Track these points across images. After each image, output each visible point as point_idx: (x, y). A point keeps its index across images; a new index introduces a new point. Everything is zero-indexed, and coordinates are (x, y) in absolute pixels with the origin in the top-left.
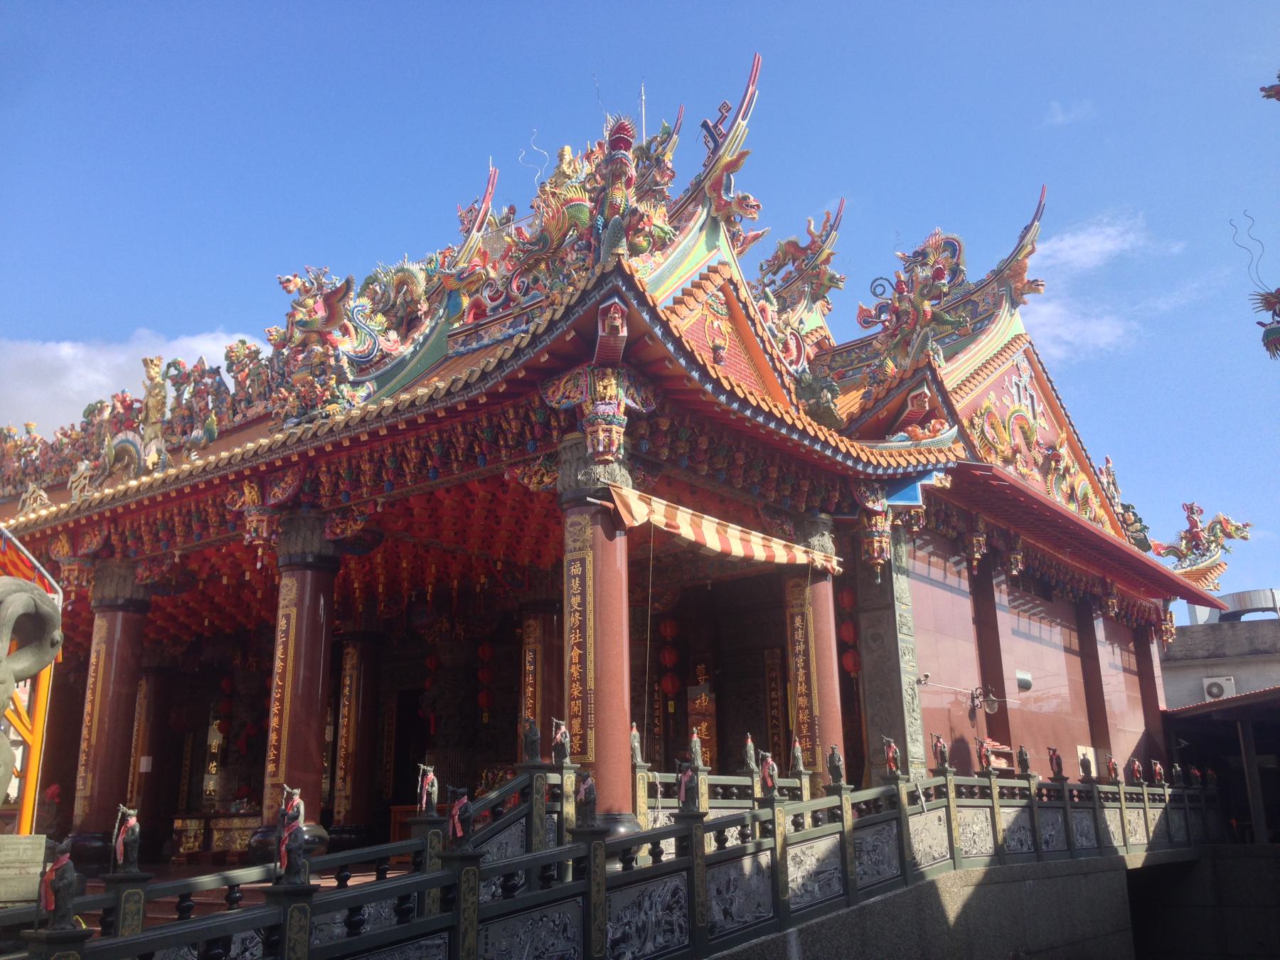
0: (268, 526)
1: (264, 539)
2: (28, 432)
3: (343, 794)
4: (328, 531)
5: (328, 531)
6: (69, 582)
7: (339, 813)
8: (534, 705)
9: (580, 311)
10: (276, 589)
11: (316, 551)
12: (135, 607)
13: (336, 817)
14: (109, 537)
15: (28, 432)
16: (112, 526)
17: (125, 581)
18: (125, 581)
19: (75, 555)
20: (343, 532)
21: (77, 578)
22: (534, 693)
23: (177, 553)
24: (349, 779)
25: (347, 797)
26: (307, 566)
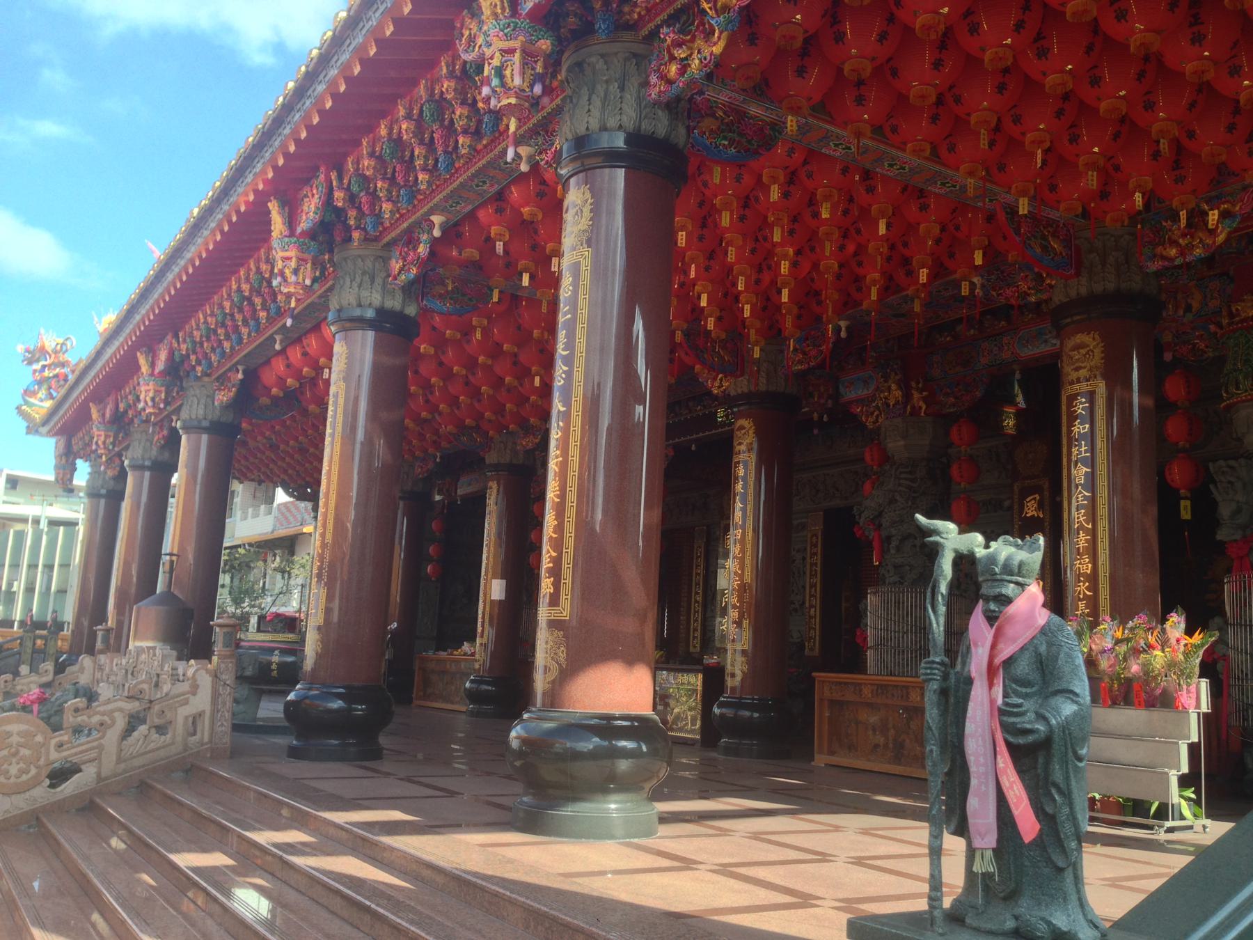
0: (524, 64)
1: (519, 93)
2: (1096, 927)
3: (739, 647)
4: (653, 79)
5: (653, 79)
6: (285, 279)
7: (733, 675)
8: (1093, 542)
9: (1214, 194)
10: (554, 209)
11: (630, 124)
12: (393, 328)
13: (729, 682)
14: (330, 190)
15: (1096, 927)
16: (334, 175)
17: (373, 280)
18: (373, 280)
19: (292, 234)
20: (683, 70)
21: (296, 272)
22: (1092, 477)
23: (437, 219)
24: (746, 623)
25: (744, 652)
26: (612, 158)
